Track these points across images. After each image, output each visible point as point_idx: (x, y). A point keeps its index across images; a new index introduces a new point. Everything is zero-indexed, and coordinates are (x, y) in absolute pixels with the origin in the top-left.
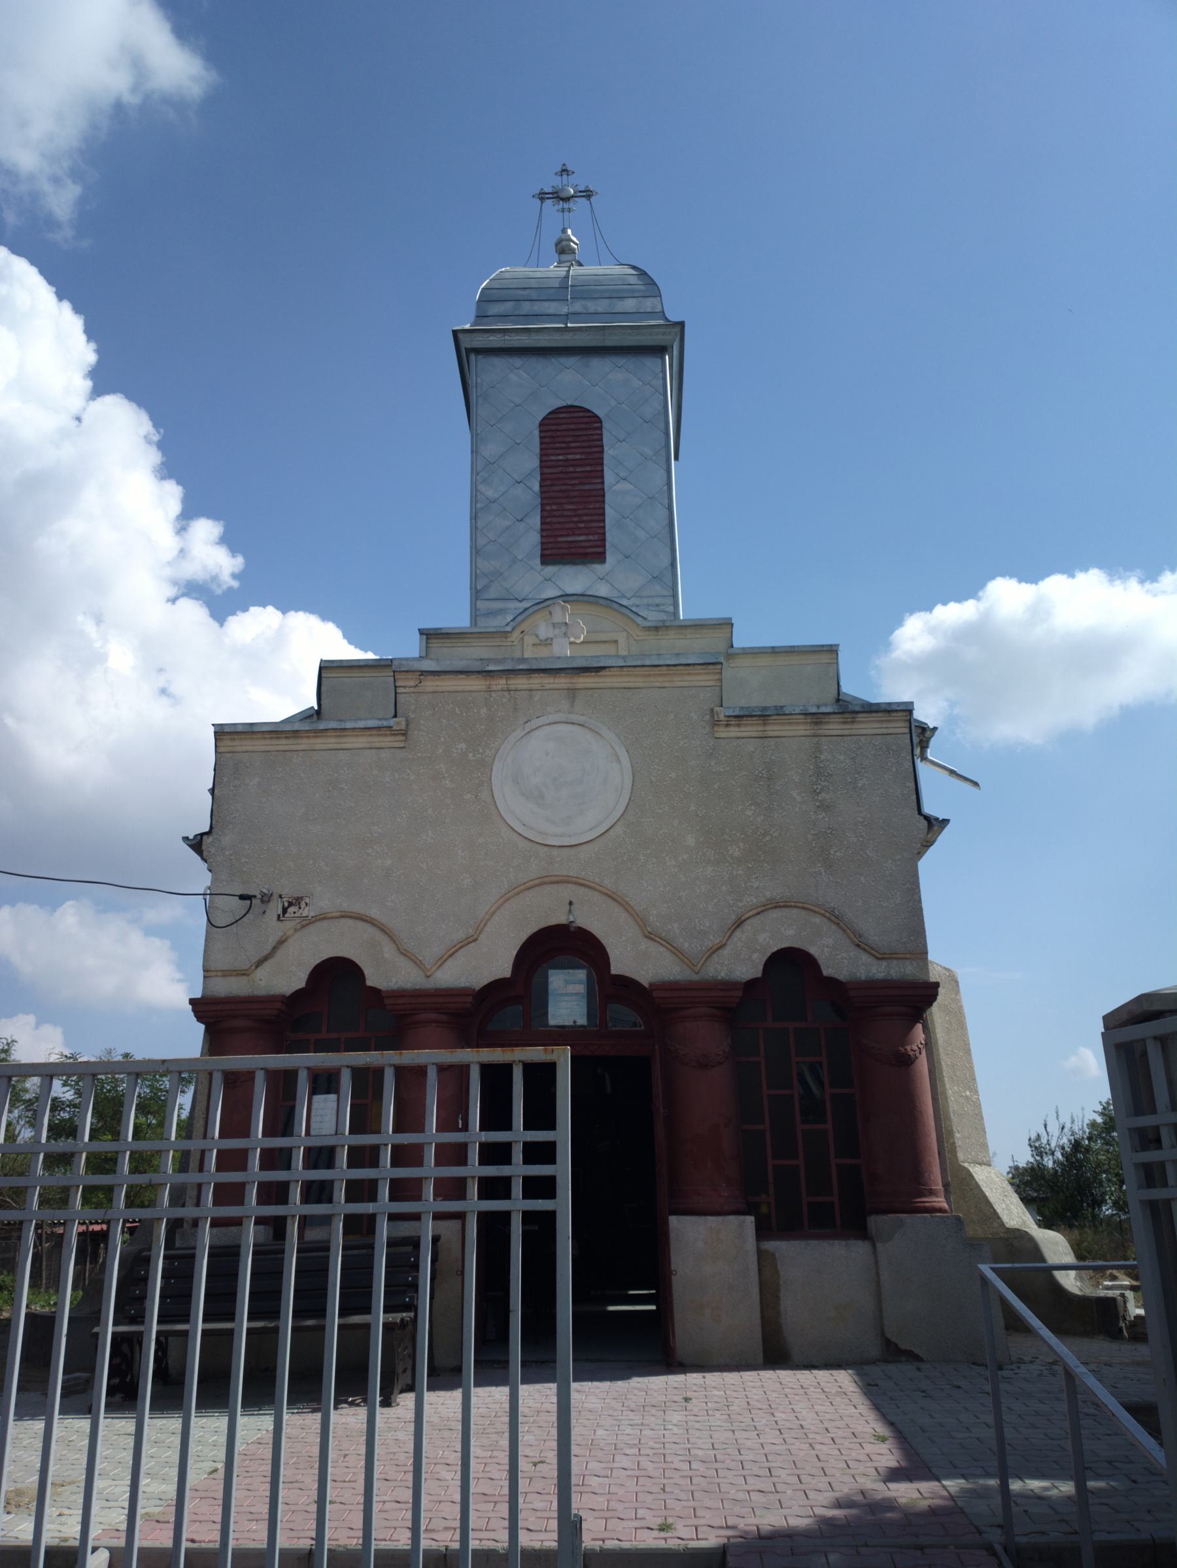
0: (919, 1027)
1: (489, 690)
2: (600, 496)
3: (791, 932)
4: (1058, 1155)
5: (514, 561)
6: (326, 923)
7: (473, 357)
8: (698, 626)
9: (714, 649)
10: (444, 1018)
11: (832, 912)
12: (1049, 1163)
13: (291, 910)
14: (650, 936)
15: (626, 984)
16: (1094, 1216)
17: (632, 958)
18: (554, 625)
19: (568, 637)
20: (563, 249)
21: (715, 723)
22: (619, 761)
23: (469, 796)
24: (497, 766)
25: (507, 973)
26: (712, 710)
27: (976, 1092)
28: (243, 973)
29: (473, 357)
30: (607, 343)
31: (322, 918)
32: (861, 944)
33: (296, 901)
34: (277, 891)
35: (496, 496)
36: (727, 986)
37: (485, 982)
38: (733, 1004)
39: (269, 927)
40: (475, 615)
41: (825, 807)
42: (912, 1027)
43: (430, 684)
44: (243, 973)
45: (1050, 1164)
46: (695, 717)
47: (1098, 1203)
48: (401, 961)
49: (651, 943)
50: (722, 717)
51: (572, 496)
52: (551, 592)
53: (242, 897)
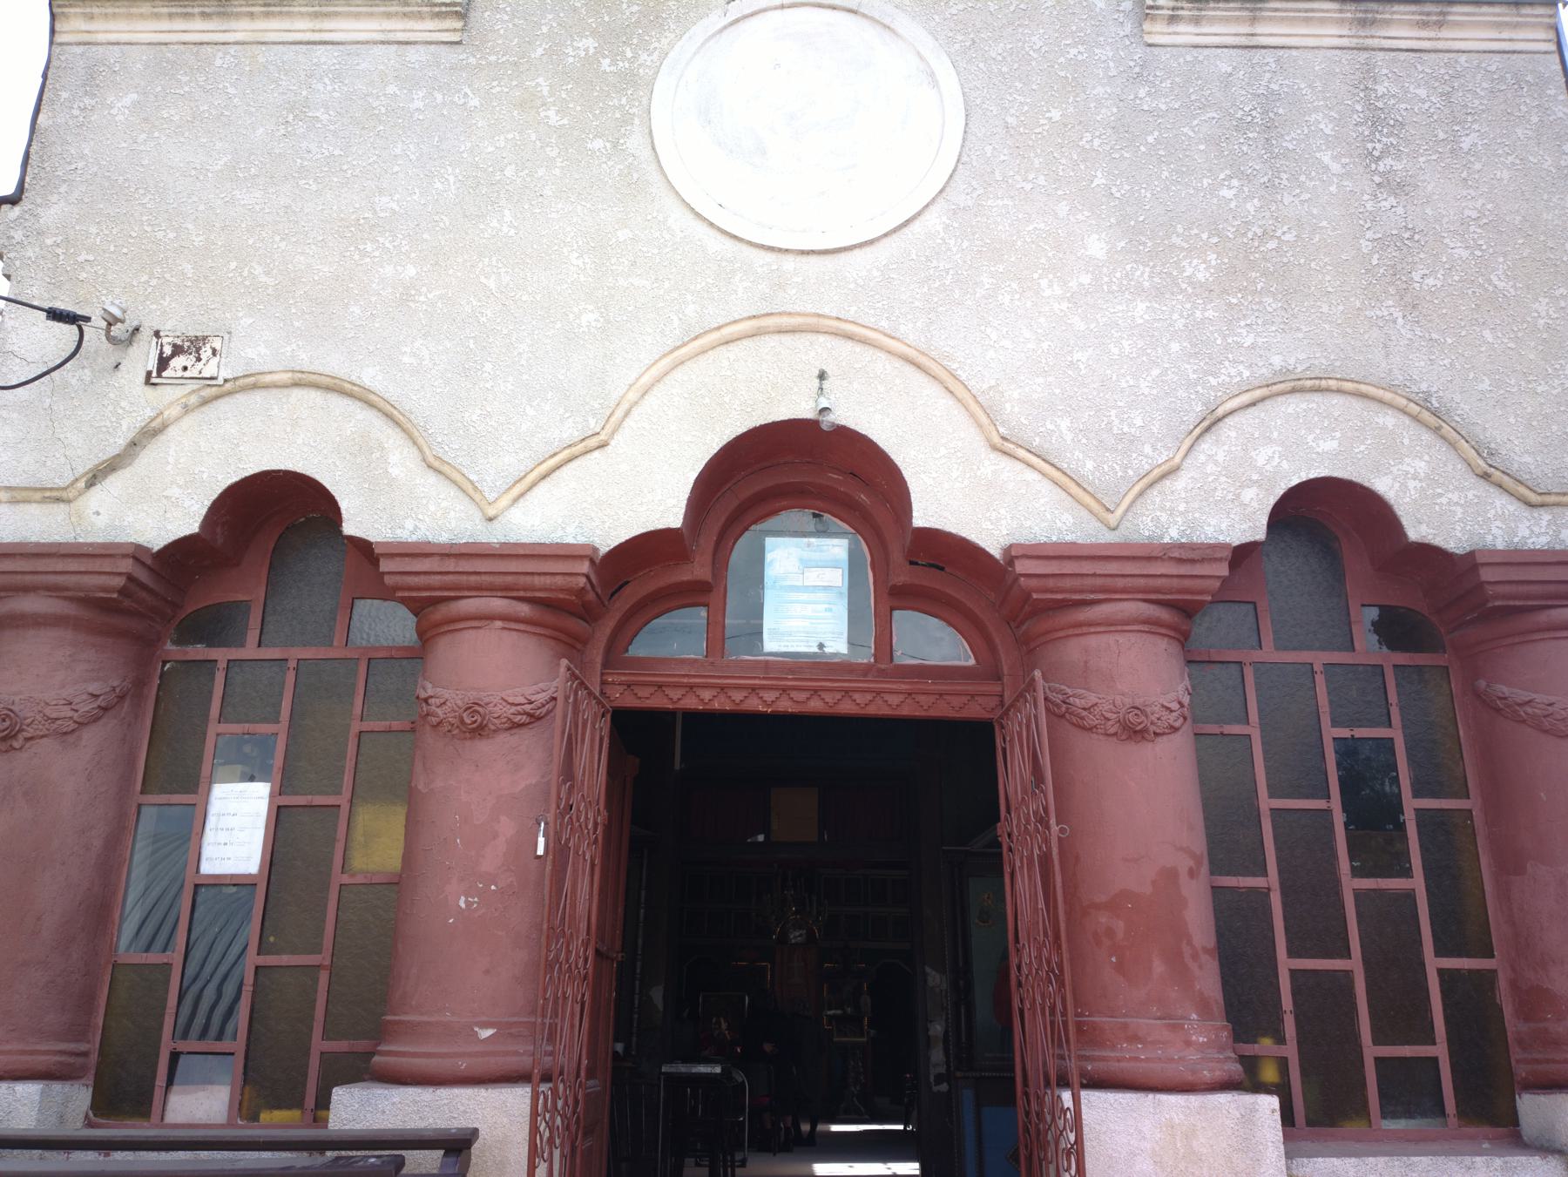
3: (1329, 445)
6: (258, 396)
10: (524, 609)
11: (1424, 402)
13: (178, 362)
14: (1004, 447)
17: (963, 493)
22: (934, 81)
23: (598, 144)
24: (663, 85)
28: (55, 496)
31: (250, 384)
33: (192, 346)
38: (1190, 597)
44: (55, 496)
49: (1005, 462)
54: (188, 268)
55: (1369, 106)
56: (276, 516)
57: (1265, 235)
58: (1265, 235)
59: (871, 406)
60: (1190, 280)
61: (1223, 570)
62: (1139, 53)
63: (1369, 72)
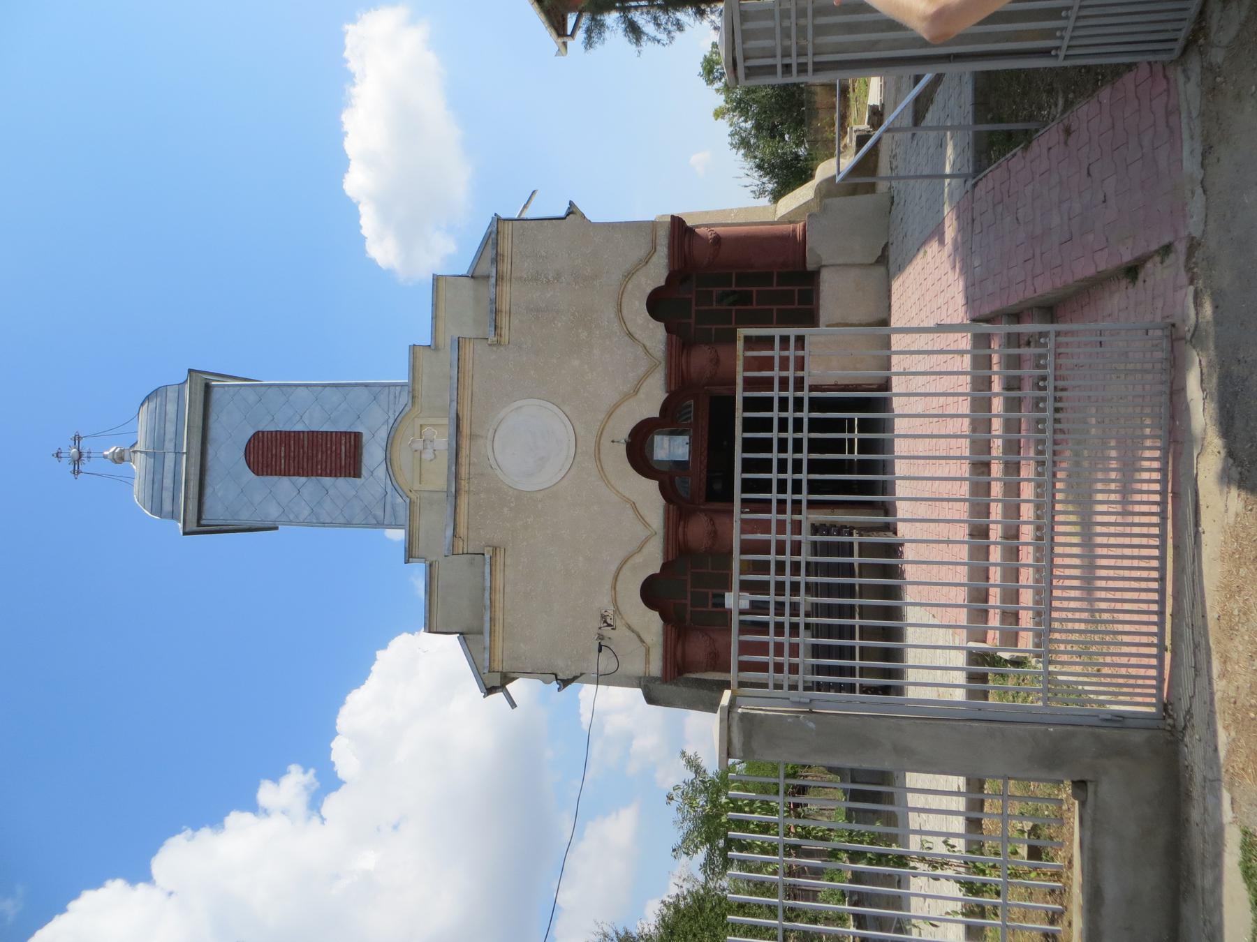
1: (469, 492)
2: (313, 434)
3: (637, 303)
4: (765, 180)
7: (203, 522)
12: (770, 187)
16: (806, 160)
17: (650, 403)
20: (120, 458)
21: (499, 344)
25: (657, 483)
29: (203, 522)
33: (604, 618)
34: (596, 630)
36: (669, 344)
38: (682, 341)
39: (619, 636)
41: (558, 277)
43: (462, 531)
47: (797, 157)
48: (645, 551)
51: (312, 454)
53: (600, 651)
56: (652, 593)
59: (623, 427)
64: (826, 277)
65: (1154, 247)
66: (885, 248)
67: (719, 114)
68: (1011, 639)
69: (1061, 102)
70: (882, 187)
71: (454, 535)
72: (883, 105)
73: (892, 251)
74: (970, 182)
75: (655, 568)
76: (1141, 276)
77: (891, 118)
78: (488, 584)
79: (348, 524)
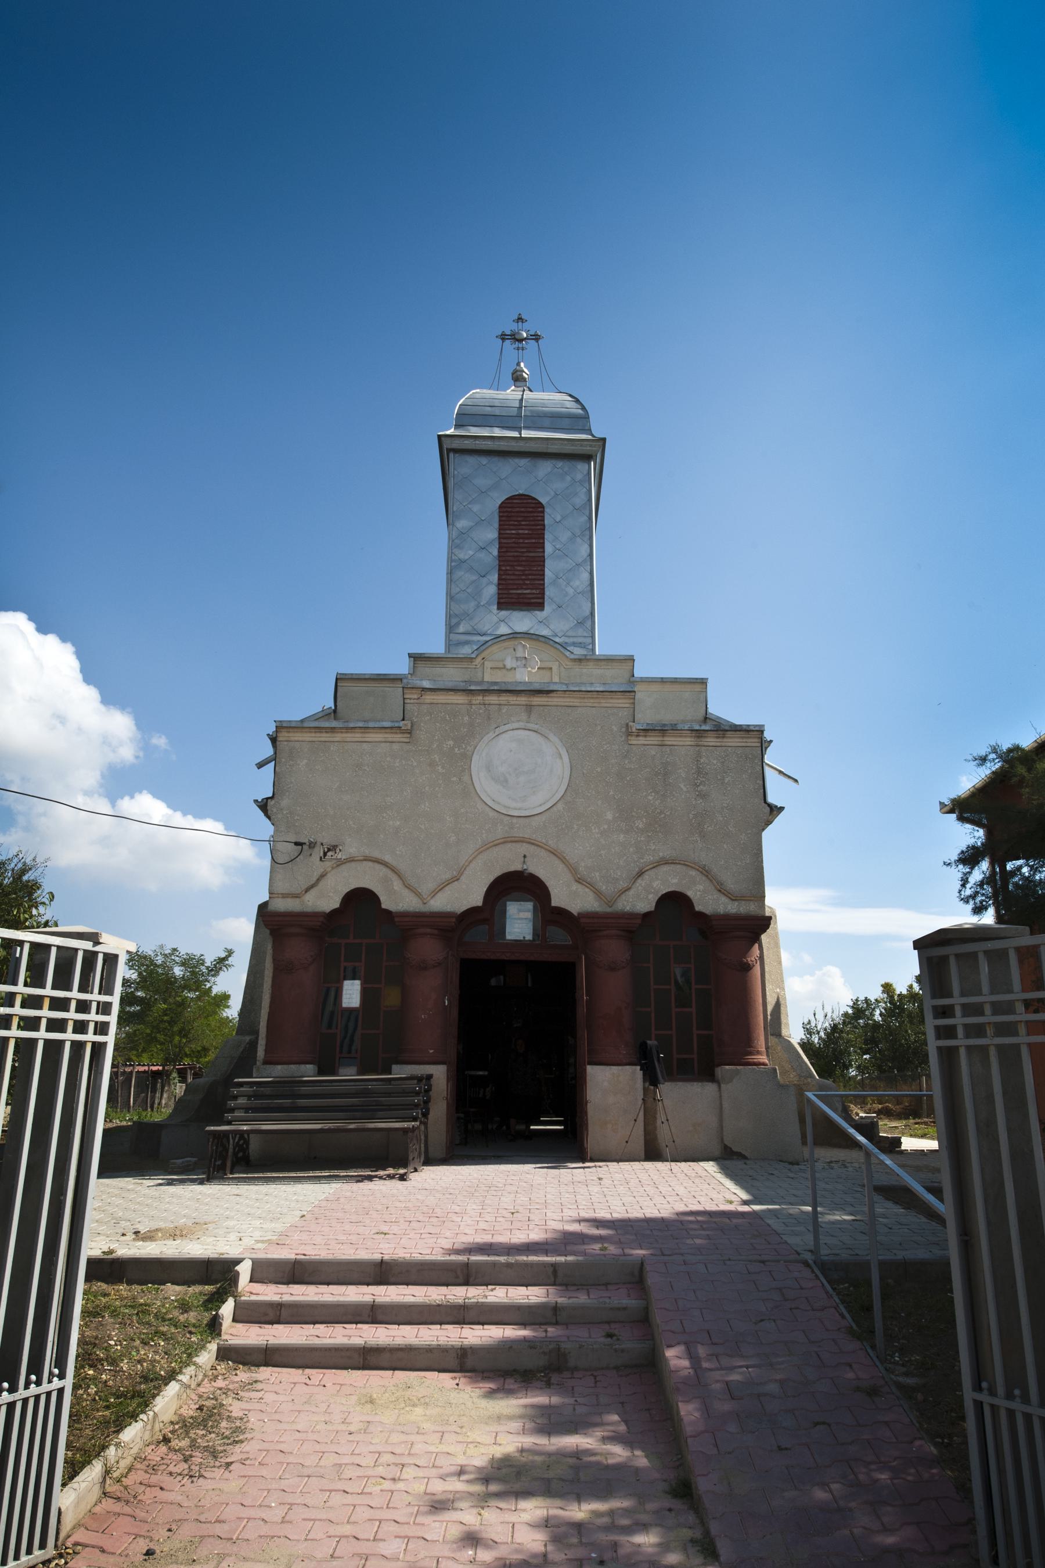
0: (757, 945)
1: (470, 704)
2: (541, 561)
3: (675, 881)
4: (822, 1034)
5: (478, 606)
6: (353, 864)
7: (451, 455)
8: (609, 660)
9: (624, 682)
10: (436, 932)
11: (704, 868)
12: (815, 1039)
13: (330, 854)
14: (579, 881)
15: (562, 913)
16: (843, 1076)
17: (568, 896)
18: (517, 659)
19: (527, 669)
20: (517, 378)
21: (629, 734)
22: (561, 758)
23: (454, 779)
24: (475, 758)
25: (480, 903)
26: (627, 725)
27: (784, 989)
28: (296, 896)
29: (451, 455)
30: (550, 451)
31: (351, 860)
32: (722, 890)
33: (333, 848)
34: (319, 840)
35: (467, 557)
36: (631, 916)
37: (464, 908)
38: (633, 928)
39: (314, 864)
40: (449, 644)
41: (702, 796)
42: (753, 945)
43: (428, 698)
44: (296, 896)
45: (816, 1041)
46: (615, 729)
47: (847, 1067)
48: (406, 892)
49: (580, 886)
50: (634, 730)
51: (521, 560)
52: (503, 630)
53: (296, 844)
54: (329, 822)
55: (698, 768)
56: (360, 899)
57: (661, 812)
58: (661, 812)
59: (541, 868)
60: (637, 827)
61: (639, 921)
62: (626, 747)
63: (699, 755)
64: (710, 1088)
65: (714, 1528)
66: (741, 1156)
67: (887, 988)
68: (248, 1314)
69: (910, 1381)
70: (806, 1152)
71: (424, 689)
72: (902, 1152)
73: (739, 1164)
74: (809, 1257)
75: (386, 904)
76: (677, 1504)
77: (888, 1162)
78: (371, 725)
79: (451, 597)
